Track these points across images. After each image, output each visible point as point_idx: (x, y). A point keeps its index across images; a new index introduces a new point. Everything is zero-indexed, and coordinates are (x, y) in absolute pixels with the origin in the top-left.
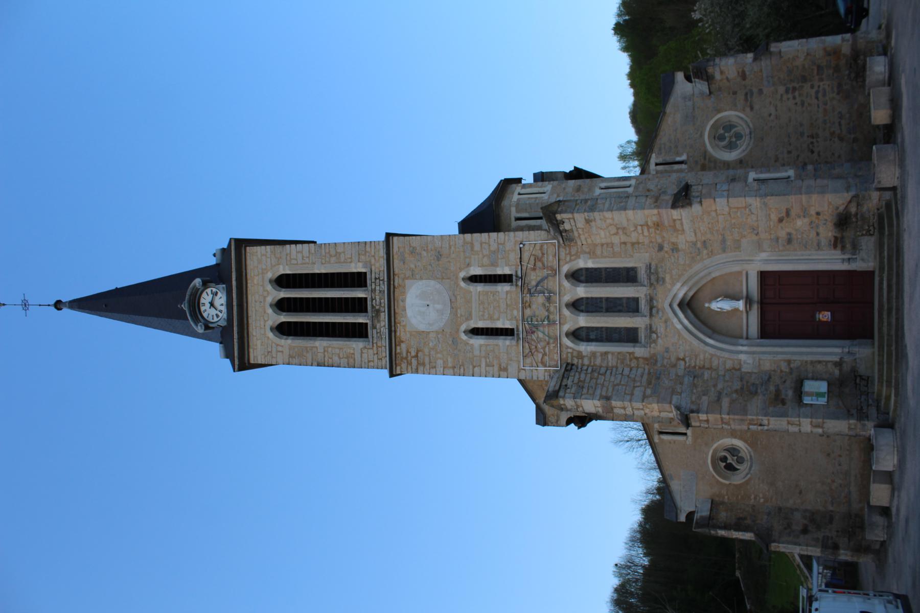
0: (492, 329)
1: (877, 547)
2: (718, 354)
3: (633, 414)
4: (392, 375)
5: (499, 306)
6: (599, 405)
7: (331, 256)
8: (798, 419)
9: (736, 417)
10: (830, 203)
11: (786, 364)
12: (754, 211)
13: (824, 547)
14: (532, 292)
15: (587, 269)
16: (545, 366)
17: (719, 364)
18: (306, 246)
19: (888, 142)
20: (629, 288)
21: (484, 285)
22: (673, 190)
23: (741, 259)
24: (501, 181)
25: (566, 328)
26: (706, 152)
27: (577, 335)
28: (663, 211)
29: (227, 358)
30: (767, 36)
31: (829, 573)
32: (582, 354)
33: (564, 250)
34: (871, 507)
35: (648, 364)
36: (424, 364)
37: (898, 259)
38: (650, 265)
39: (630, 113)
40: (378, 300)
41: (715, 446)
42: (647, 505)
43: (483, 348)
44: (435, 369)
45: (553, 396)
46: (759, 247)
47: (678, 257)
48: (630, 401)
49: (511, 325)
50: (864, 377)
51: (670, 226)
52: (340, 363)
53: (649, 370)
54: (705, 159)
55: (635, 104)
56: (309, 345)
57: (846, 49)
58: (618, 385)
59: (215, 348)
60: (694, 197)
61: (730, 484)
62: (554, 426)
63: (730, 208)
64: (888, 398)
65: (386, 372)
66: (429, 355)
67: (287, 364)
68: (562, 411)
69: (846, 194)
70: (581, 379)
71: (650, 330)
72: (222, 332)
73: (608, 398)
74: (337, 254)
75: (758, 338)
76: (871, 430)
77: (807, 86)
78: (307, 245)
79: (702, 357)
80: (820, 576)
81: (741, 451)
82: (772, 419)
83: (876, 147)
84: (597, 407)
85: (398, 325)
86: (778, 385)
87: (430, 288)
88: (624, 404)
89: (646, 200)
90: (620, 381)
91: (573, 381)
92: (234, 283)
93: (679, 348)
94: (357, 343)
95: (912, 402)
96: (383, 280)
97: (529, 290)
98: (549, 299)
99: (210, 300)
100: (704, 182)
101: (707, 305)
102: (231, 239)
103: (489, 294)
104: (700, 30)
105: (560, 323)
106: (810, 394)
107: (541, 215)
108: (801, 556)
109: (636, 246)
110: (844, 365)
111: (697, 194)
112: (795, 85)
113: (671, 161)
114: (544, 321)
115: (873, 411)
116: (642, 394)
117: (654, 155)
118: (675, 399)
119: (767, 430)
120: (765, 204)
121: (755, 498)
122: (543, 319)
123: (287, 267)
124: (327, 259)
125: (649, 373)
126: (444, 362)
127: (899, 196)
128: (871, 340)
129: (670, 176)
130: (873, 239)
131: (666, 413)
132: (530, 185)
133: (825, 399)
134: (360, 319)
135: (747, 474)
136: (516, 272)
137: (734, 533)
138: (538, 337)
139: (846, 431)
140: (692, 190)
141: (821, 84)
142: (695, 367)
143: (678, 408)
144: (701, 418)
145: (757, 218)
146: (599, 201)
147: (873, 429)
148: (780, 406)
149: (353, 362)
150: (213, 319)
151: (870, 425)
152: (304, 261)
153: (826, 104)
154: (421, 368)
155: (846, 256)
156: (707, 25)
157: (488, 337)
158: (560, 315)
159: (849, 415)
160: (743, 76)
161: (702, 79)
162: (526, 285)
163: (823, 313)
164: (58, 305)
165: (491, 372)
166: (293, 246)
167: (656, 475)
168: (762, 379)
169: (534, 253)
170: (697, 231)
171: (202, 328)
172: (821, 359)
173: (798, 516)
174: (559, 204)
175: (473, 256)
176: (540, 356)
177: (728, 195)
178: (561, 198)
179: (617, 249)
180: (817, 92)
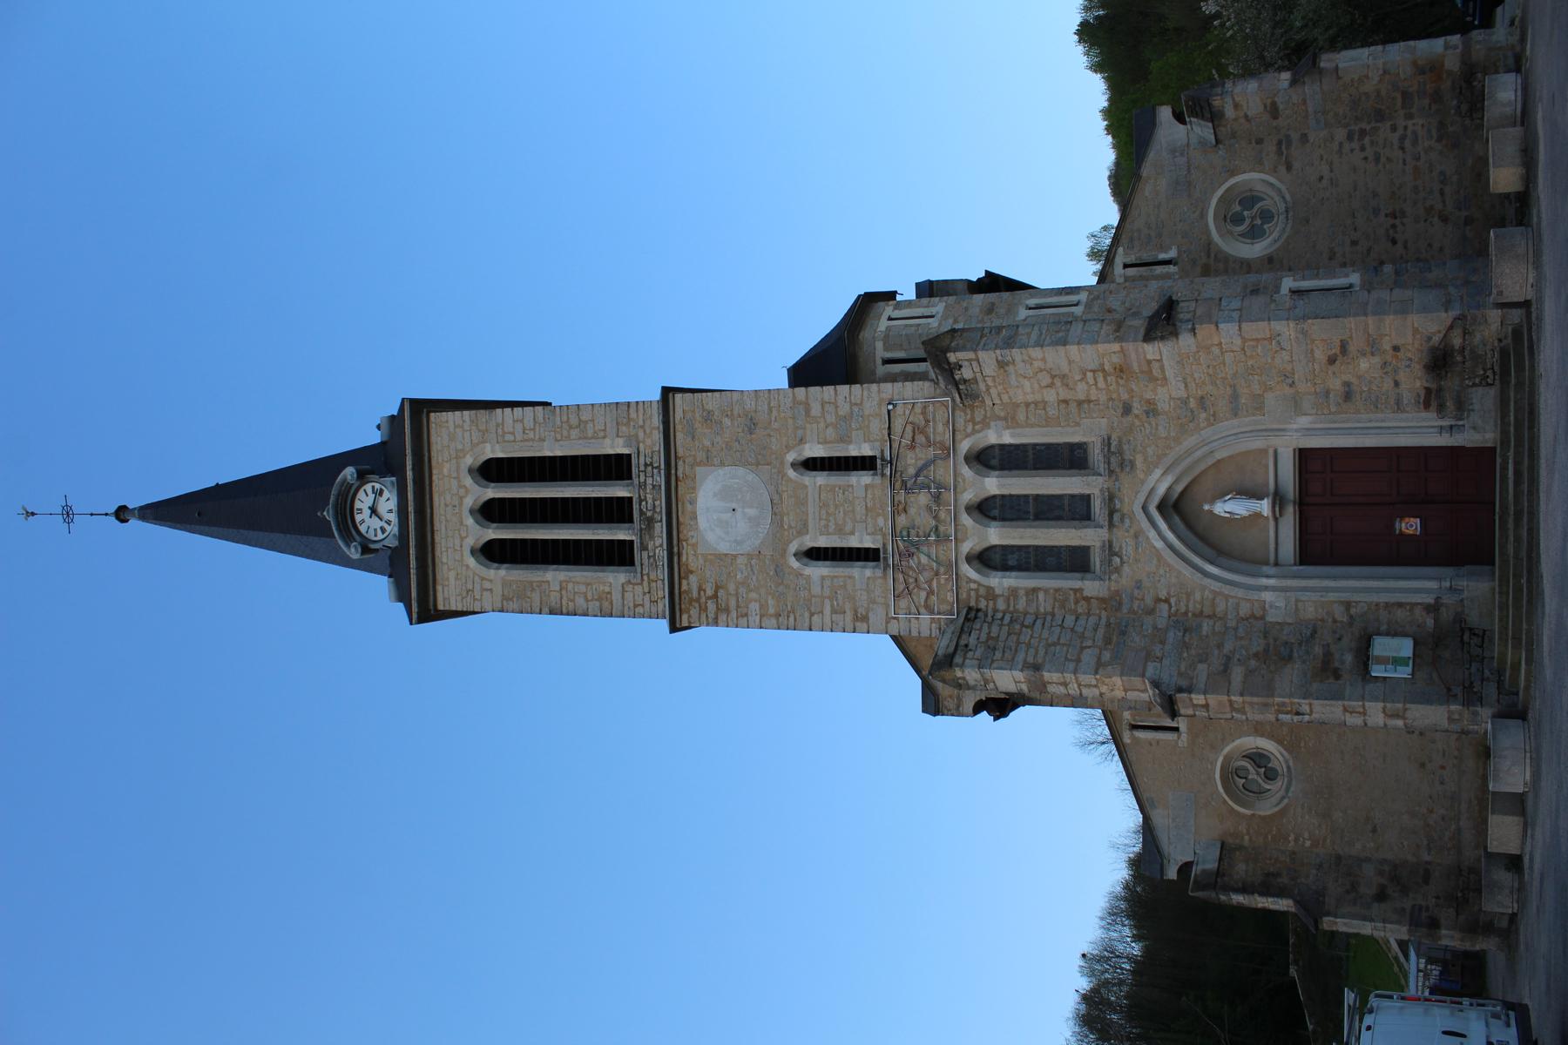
0: (842, 549)
1: (1504, 924)
4: (674, 628)
5: (853, 511)
8: (1361, 703)
9: (1255, 699)
10: (1415, 331)
11: (1342, 608)
12: (1285, 345)
13: (1414, 923)
14: (908, 486)
15: (1002, 447)
16: (932, 613)
17: (1227, 608)
18: (528, 410)
19: (1520, 224)
23: (1264, 427)
24: (859, 296)
25: (966, 547)
26: (1209, 243)
27: (986, 559)
28: (1130, 347)
33: (963, 414)
34: (1491, 856)
35: (1105, 609)
36: (727, 610)
37: (1531, 427)
38: (1109, 439)
40: (650, 501)
43: (827, 583)
45: (945, 662)
46: (1296, 406)
47: (1157, 425)
48: (1075, 672)
49: (873, 543)
51: (1142, 372)
54: (1209, 256)
55: (1118, 163)
57: (1452, 63)
58: (1054, 644)
59: (379, 585)
60: (1181, 321)
61: (1253, 815)
62: (952, 715)
63: (1244, 340)
64: (1516, 667)
65: (664, 624)
66: (737, 594)
67: (499, 611)
69: (1444, 315)
70: (992, 635)
71: (1110, 550)
72: (391, 558)
73: (1037, 668)
75: (1295, 564)
76: (1487, 722)
78: (531, 408)
79: (1198, 596)
80: (1421, 974)
81: (1272, 757)
82: (1316, 702)
84: (1019, 682)
85: (684, 543)
86: (1328, 645)
90: (1059, 639)
91: (978, 639)
92: (409, 474)
93: (1159, 581)
94: (616, 574)
96: (658, 467)
97: (904, 483)
98: (937, 498)
99: (370, 504)
101: (1206, 507)
102: (403, 399)
103: (837, 489)
106: (1383, 661)
110: (1443, 609)
111: (1188, 316)
112: (1364, 125)
115: (1491, 690)
119: (1308, 722)
120: (1304, 333)
121: (1296, 840)
122: (928, 531)
125: (1108, 625)
126: (761, 607)
127: (1534, 315)
128: (1491, 567)
129: (1146, 286)
131: (1136, 693)
132: (909, 304)
133: (1409, 669)
134: (621, 534)
136: (882, 451)
138: (919, 562)
139: (1445, 724)
140: (1179, 310)
141: (1410, 123)
142: (1186, 613)
143: (1156, 684)
144: (1195, 702)
145: (1292, 357)
146: (1020, 329)
148: (1331, 680)
150: (376, 535)
151: (1485, 713)
152: (525, 437)
153: (1418, 159)
154: (723, 617)
155: (1446, 423)
158: (956, 525)
159: (1448, 696)
160: (1274, 111)
161: (1203, 118)
162: (898, 474)
163: (1407, 519)
164: (122, 514)
165: (841, 623)
166: (508, 411)
168: (1301, 634)
170: (1189, 380)
175: (808, 426)
176: (923, 595)
178: (959, 326)
179: (1052, 412)
180: (1402, 138)
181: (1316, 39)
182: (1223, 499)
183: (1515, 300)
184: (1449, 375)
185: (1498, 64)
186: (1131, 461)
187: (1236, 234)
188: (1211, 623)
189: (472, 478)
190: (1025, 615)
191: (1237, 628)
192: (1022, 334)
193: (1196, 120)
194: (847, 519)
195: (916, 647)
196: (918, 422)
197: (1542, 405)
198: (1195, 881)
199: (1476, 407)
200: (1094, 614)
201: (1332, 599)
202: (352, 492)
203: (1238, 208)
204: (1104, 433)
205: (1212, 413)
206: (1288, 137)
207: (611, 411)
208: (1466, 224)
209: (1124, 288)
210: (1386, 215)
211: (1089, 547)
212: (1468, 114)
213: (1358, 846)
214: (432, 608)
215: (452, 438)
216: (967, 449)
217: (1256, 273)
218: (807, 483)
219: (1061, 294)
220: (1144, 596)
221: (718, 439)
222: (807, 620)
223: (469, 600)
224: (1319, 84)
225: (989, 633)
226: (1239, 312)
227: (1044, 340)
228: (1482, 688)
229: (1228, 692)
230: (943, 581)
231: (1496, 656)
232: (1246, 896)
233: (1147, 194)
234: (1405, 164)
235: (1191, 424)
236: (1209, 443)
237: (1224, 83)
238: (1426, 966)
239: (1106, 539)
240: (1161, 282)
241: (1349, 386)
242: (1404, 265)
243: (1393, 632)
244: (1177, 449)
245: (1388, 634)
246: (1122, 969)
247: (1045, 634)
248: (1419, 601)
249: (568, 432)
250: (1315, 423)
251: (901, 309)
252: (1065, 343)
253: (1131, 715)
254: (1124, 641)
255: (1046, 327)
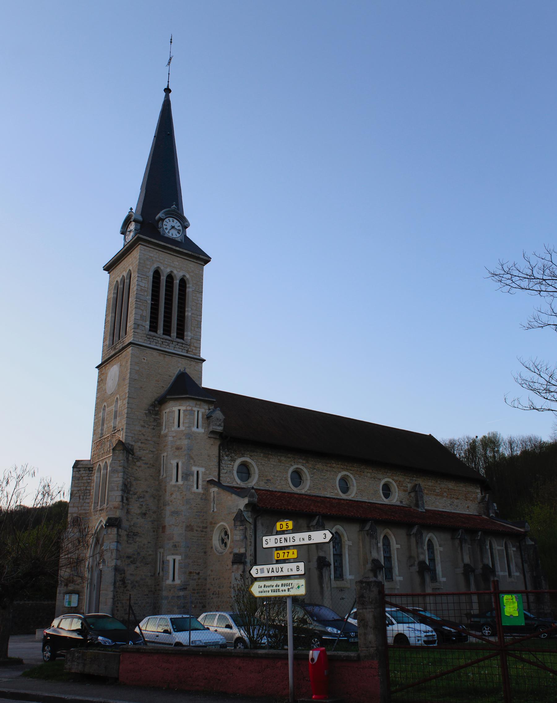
26: (216, 524)
106: (70, 598)
116: (74, 512)
133: (67, 606)
164: (168, 91)
202: (180, 221)
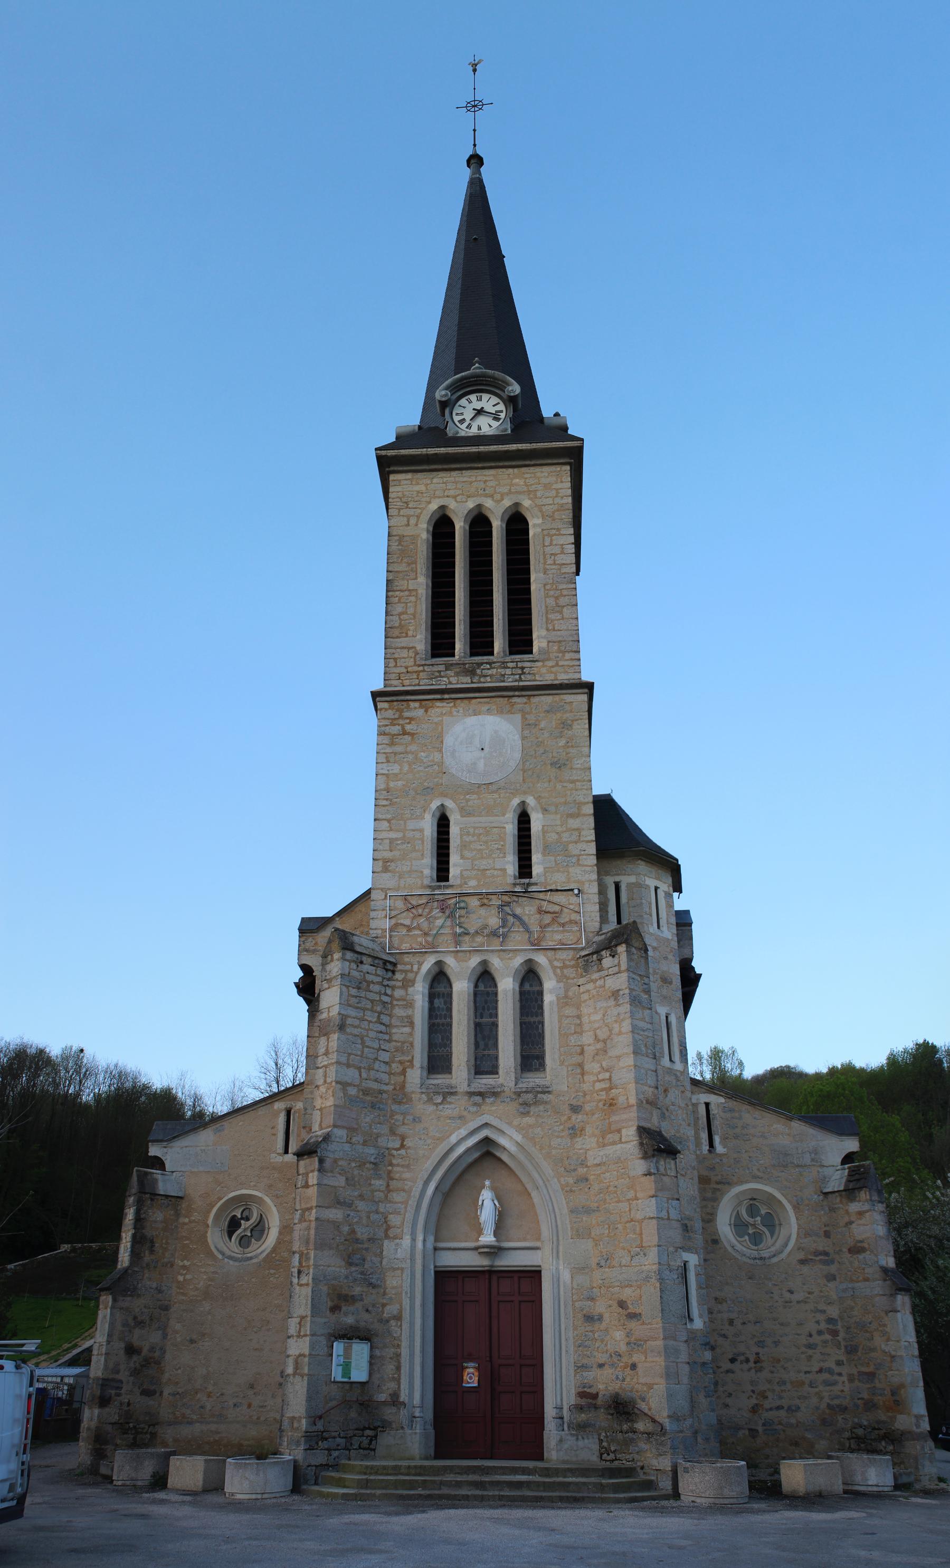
0: (448, 848)
1: (103, 1470)
2: (410, 1202)
3: (318, 1068)
4: (375, 695)
5: (482, 858)
6: (331, 1014)
7: (557, 598)
8: (308, 1333)
9: (312, 1232)
10: (650, 1386)
11: (395, 1312)
12: (636, 1260)
13: (105, 1383)
14: (505, 908)
15: (541, 993)
16: (391, 930)
17: (396, 1203)
18: (572, 559)
19: (752, 1486)
20: (512, 1059)
21: (514, 835)
22: (668, 1130)
23: (561, 1238)
24: (677, 860)
25: (450, 961)
26: (730, 1184)
27: (440, 978)
28: (633, 1114)
29: (397, 438)
30: (920, 1294)
31: (63, 1394)
32: (410, 987)
33: (570, 957)
34: (167, 1457)
35: (395, 1089)
36: (392, 744)
37: (561, 1499)
38: (549, 1092)
39: (788, 1067)
40: (490, 672)
41: (267, 1200)
42: (176, 1098)
43: (418, 835)
44: (384, 761)
45: (346, 943)
46: (579, 1269)
47: (562, 1137)
48: (338, 1063)
49: (453, 876)
50: (374, 1442)
51: (610, 1124)
52: (392, 615)
53: (385, 1092)
54: (718, 1183)
55: (802, 1075)
56: (419, 566)
57: (902, 1422)
58: (363, 1043)
59: (412, 418)
60: (657, 1162)
61: (208, 1226)
62: (300, 945)
63: (641, 1222)
64: (340, 1483)
65: (379, 685)
66: (406, 752)
67: (389, 533)
68: (322, 957)
69: (665, 1414)
70: (372, 985)
71: (449, 1093)
72: (436, 428)
73: (342, 1027)
74: (559, 608)
75: (435, 1267)
76: (290, 1455)
77: (841, 1355)
78: (574, 561)
79: (407, 1175)
80: (59, 1380)
81: (260, 1242)
82: (309, 1289)
83: (742, 1466)
84: (329, 1011)
85: (452, 704)
86: (362, 1300)
87: (509, 752)
88: (333, 1052)
89: (650, 1087)
90: (368, 1047)
91: (368, 973)
92: (514, 447)
93: (420, 1139)
94: (424, 641)
95: (334, 1521)
96: (521, 680)
97: (508, 904)
98: (494, 934)
99: (486, 409)
100: (681, 1181)
101: (487, 1183)
102: (582, 440)
103: (502, 843)
104: (929, 1182)
105: (458, 951)
106: (347, 1353)
107: (624, 922)
108: (89, 1350)
109: (579, 1071)
110: (394, 1410)
111: (662, 1169)
112: (842, 1334)
113: (713, 1128)
114: (461, 927)
115: (320, 1458)
116: (349, 1081)
117: (722, 1100)
118: (341, 1133)
119: (291, 1282)
120: (647, 1279)
121: (184, 1267)
122: (464, 925)
123: (539, 530)
124: (552, 593)
125: (381, 1092)
126: (396, 775)
127: (664, 1503)
128: (433, 1454)
129: (689, 1125)
130: (595, 1458)
131: (319, 1120)
132: (670, 905)
133: (339, 1378)
134: (460, 645)
135: (223, 1254)
136: (536, 884)
137: (130, 1234)
138: (436, 918)
139: (289, 1414)
140: (668, 1160)
141: (845, 1378)
142: (391, 1164)
143: (327, 1138)
144: (310, 1175)
145: (625, 1266)
146: (648, 1011)
147: (291, 1457)
148: (330, 1304)
149: (394, 635)
150: (457, 414)
151: (298, 1453)
152: (548, 556)
153: (811, 1386)
154: (386, 740)
155: (566, 1413)
156: (938, 1193)
157: (435, 841)
158: (470, 951)
159: (314, 1418)
160: (857, 1249)
161: (848, 1181)
162: (515, 898)
163: (477, 1374)
164: (475, 161)
165: (381, 847)
166: (572, 539)
167: (223, 1108)
168: (372, 1274)
169: (565, 910)
170: (604, 1168)
171: (442, 396)
172: (403, 1369)
173: (155, 1337)
174: (641, 949)
175: (559, 816)
176: (407, 922)
177: (662, 1218)
178: (650, 953)
179: (573, 1040)
180: (830, 1371)
181: (926, 1278)
182: (495, 1199)
183: (680, 1485)
184: (610, 1417)
185: (902, 1466)
186: (528, 1112)
187: (739, 1209)
188: (383, 1188)
189: (510, 506)
190: (389, 1015)
191: (377, 1213)
192: (643, 1013)
193: (846, 1174)
194: (474, 853)
195: (361, 911)
196: (563, 916)
197: (582, 1513)
198: (146, 1174)
199: (580, 1443)
200: (390, 1079)
201: (404, 1303)
202: (497, 391)
203: (763, 1212)
204: (554, 1088)
205: (573, 1189)
206: (832, 1262)
207: (571, 635)
208: (751, 1430)
209: (686, 1104)
210: (757, 1354)
211: (450, 1073)
212: (854, 1435)
213: (178, 1327)
214: (392, 469)
215: (547, 487)
216: (539, 961)
217: (703, 1228)
218: (507, 816)
219: (680, 1046)
220: (407, 1124)
221: (546, 735)
222: (384, 817)
223: (398, 504)
224: (881, 1293)
225: (374, 983)
226: (666, 1217)
227: (638, 1034)
228: (322, 1449)
229: (319, 1207)
230: (419, 939)
231: (350, 1462)
232: (132, 1222)
233: (775, 1126)
234: (806, 1373)
235: (563, 1169)
236: (546, 1185)
237: (882, 1203)
238: (66, 1384)
239: (458, 1090)
240: (693, 1138)
241: (599, 1319)
242: (711, 1371)
243: (373, 1361)
244: (540, 1156)
245: (372, 1357)
246: (69, 1085)
247: (372, 1034)
248: (402, 1387)
249: (552, 596)
250: (564, 1286)
251: (665, 898)
252: (635, 1053)
253: (299, 1110)
254: (366, 1108)
255: (651, 1035)
